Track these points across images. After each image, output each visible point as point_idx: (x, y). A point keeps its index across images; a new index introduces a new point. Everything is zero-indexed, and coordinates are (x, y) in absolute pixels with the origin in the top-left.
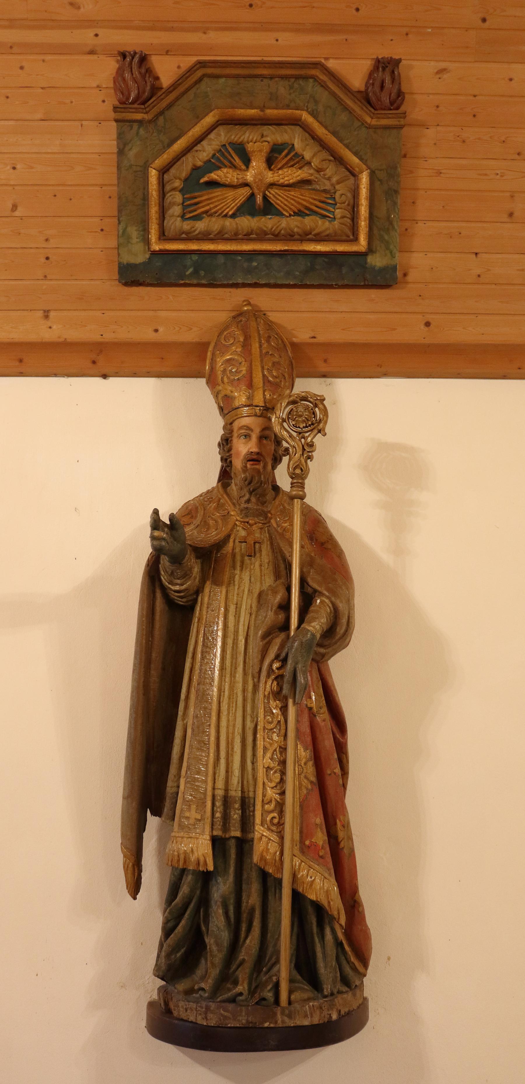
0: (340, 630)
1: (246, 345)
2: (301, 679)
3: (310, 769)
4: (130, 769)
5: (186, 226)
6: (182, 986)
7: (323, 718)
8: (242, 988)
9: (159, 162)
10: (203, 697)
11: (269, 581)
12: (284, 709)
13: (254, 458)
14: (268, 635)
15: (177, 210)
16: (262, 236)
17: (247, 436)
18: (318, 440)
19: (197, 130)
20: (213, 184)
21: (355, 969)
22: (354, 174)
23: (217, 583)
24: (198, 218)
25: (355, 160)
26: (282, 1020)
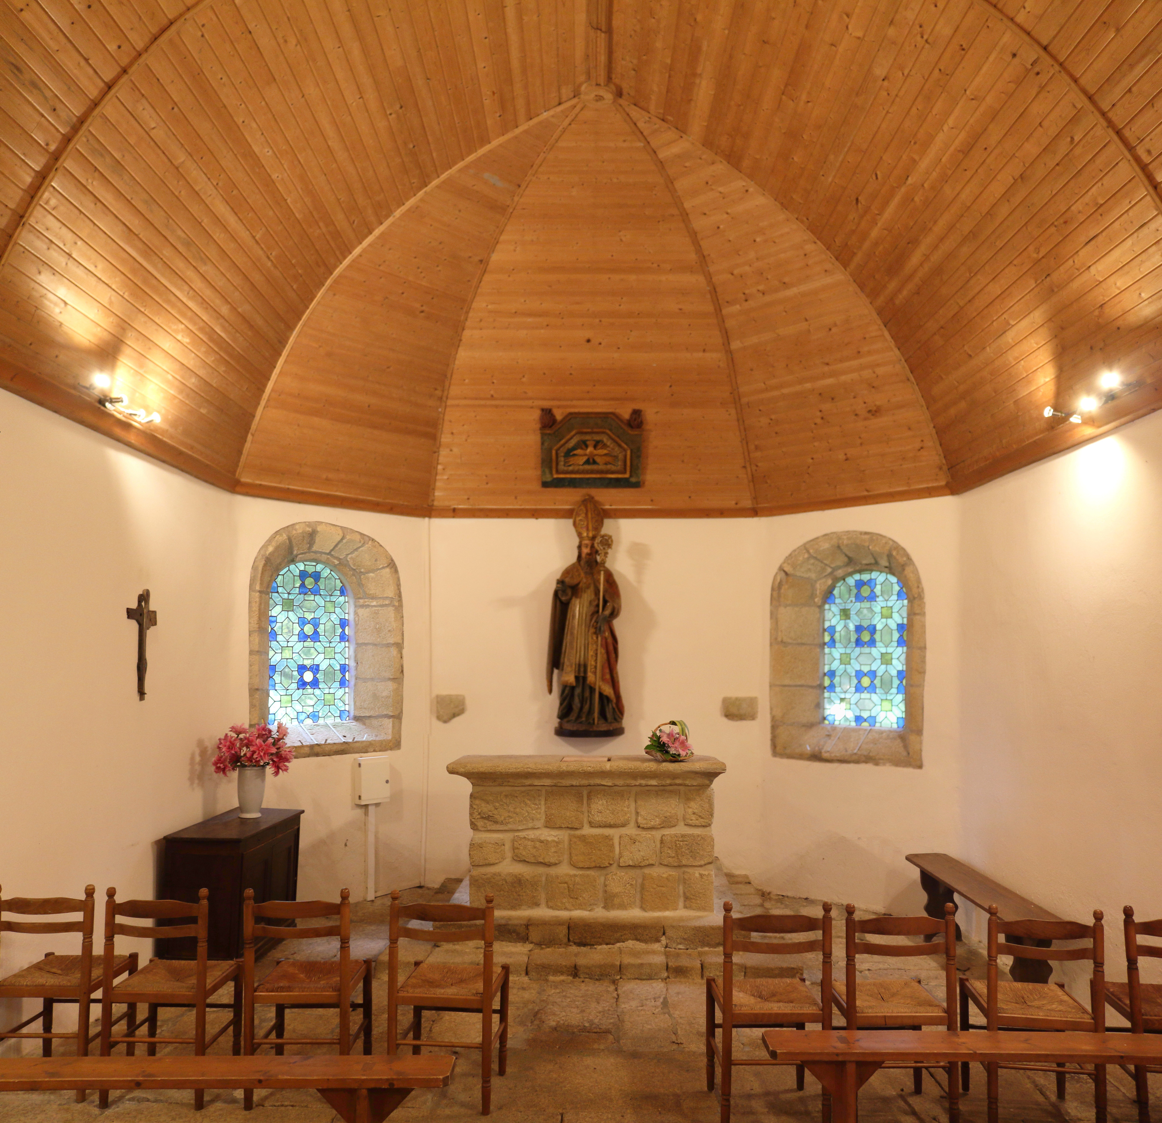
0: (615, 613)
1: (586, 514)
2: (602, 629)
3: (605, 656)
4: (549, 654)
5: (566, 468)
6: (565, 720)
7: (610, 640)
8: (584, 719)
9: (555, 448)
10: (572, 634)
11: (593, 597)
12: (597, 638)
13: (589, 554)
14: (593, 615)
15: (562, 463)
16: (592, 472)
17: (587, 547)
18: (609, 551)
19: (568, 437)
20: (575, 455)
21: (619, 717)
22: (625, 450)
23: (577, 597)
24: (570, 466)
25: (625, 446)
26: (595, 728)
